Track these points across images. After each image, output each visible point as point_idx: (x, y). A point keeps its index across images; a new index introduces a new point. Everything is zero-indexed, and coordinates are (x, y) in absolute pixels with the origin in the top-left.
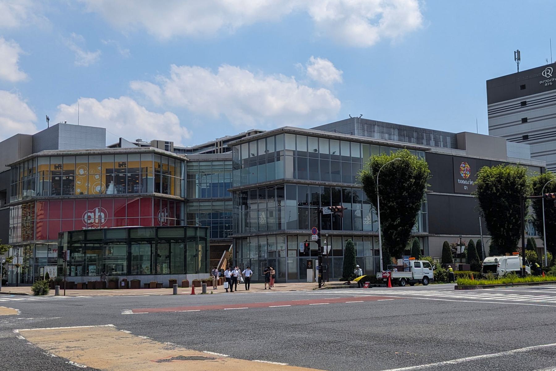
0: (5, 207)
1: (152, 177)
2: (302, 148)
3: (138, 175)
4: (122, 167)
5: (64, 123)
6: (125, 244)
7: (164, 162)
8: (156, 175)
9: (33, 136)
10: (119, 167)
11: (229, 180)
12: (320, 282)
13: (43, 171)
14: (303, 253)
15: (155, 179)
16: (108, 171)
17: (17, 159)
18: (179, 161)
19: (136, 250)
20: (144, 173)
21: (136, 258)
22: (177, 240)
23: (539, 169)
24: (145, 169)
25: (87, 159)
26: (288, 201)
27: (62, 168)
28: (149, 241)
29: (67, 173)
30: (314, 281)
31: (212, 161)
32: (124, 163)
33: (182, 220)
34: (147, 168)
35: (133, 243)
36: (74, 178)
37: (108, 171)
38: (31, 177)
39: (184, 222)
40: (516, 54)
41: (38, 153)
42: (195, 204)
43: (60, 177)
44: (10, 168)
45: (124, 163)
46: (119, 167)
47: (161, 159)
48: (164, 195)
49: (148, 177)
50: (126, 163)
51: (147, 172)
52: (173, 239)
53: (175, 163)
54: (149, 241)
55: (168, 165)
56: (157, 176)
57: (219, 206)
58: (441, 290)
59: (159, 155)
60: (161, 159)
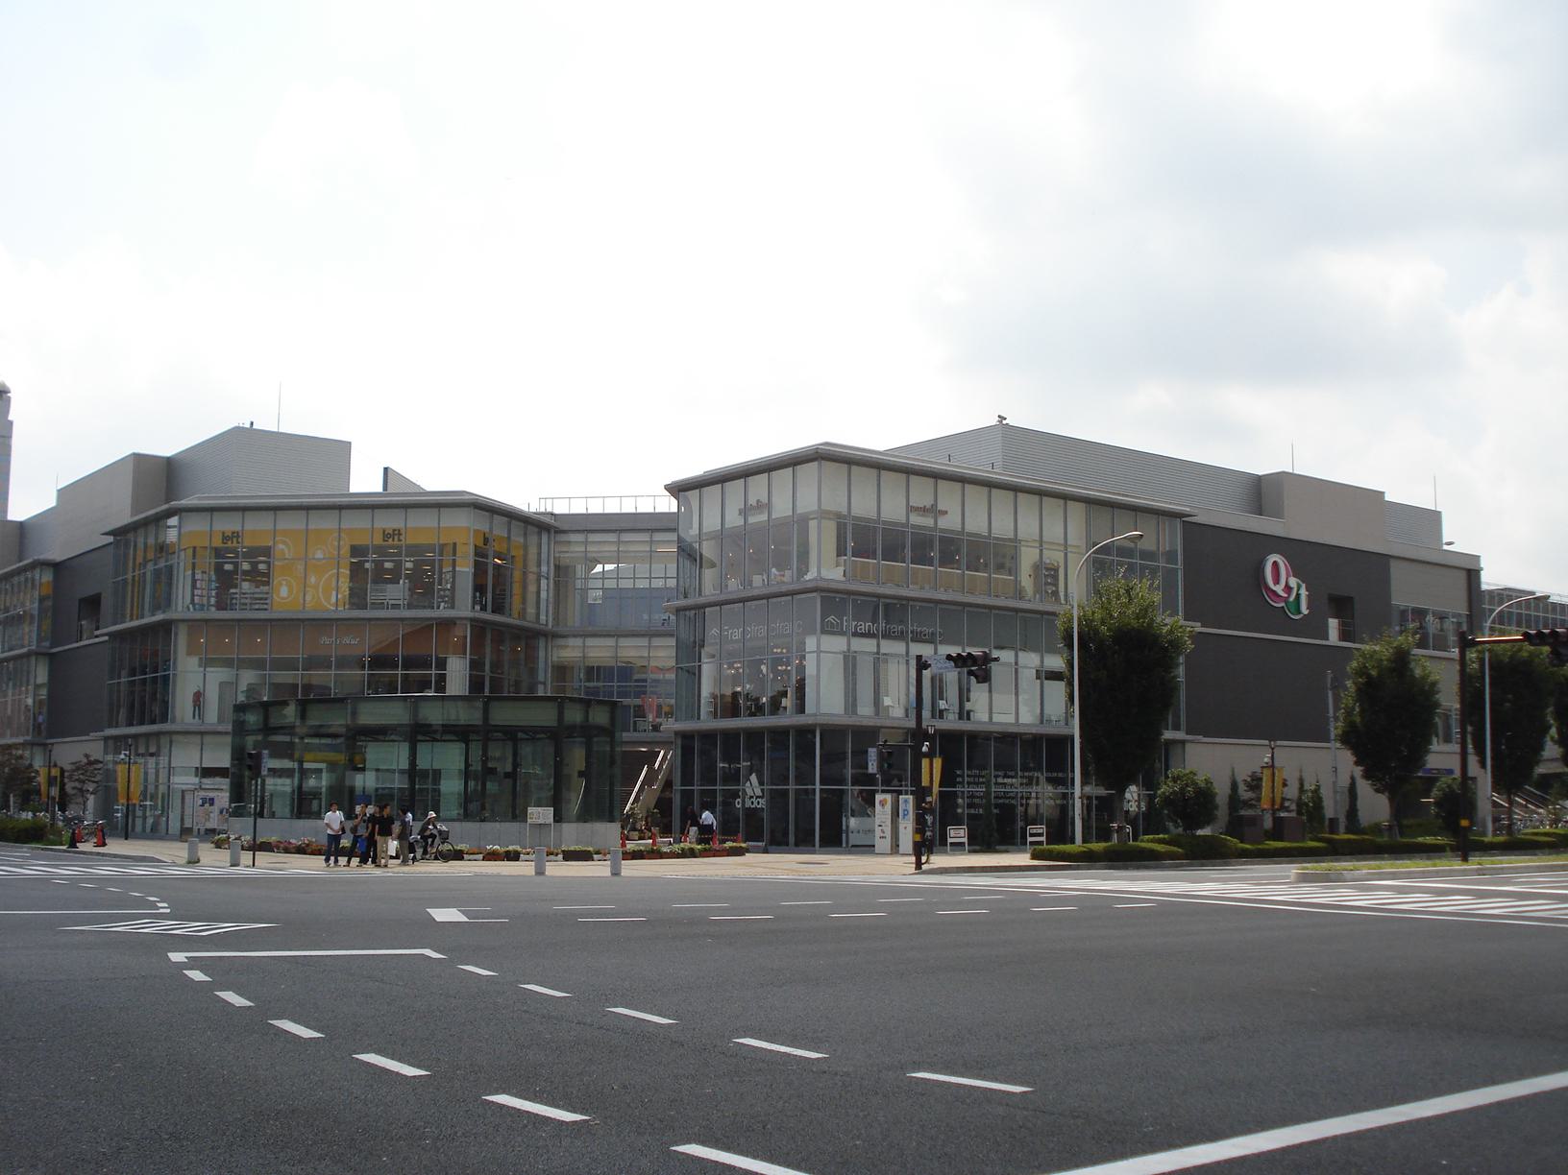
0: (97, 637)
1: (466, 568)
2: (863, 506)
3: (432, 563)
4: (391, 540)
5: (248, 426)
6: (454, 738)
7: (499, 529)
8: (476, 563)
9: (168, 458)
10: (384, 541)
11: (648, 580)
12: (918, 854)
13: (195, 548)
14: (876, 774)
15: (475, 575)
16: (356, 551)
17: (124, 517)
18: (536, 530)
19: (429, 757)
20: (447, 558)
21: (424, 774)
22: (533, 733)
23: (1463, 575)
24: (450, 549)
25: (436, 518)
26: (1330, 638)
27: (240, 540)
28: (460, 733)
29: (253, 553)
30: (895, 849)
32: (396, 532)
33: (541, 683)
34: (455, 544)
35: (420, 737)
36: (269, 567)
37: (356, 551)
38: (162, 564)
39: (545, 688)
41: (182, 502)
42: (571, 642)
43: (236, 565)
44: (111, 539)
45: (396, 532)
46: (384, 541)
47: (491, 523)
48: (497, 618)
49: (457, 569)
50: (403, 531)
51: (454, 554)
52: (524, 729)
53: (525, 534)
54: (460, 733)
55: (509, 538)
56: (480, 569)
57: (632, 650)
58: (1224, 881)
59: (487, 514)
60: (491, 523)
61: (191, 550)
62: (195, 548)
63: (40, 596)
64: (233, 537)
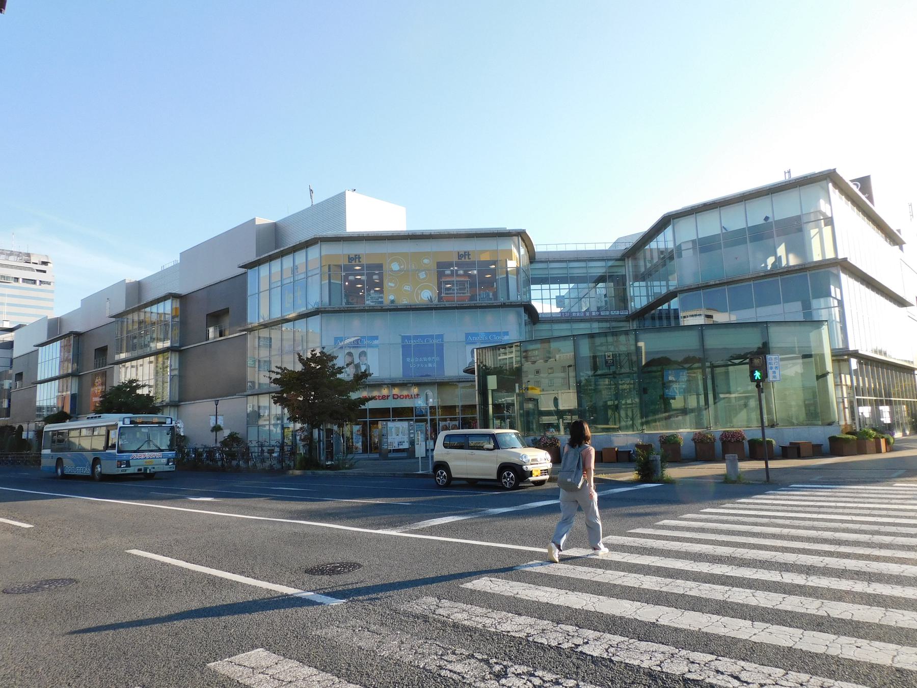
4: (463, 258)
31: (570, 261)
32: (467, 253)
40: (787, 174)
61: (328, 266)
62: (329, 265)
63: (172, 316)
64: (465, 255)
